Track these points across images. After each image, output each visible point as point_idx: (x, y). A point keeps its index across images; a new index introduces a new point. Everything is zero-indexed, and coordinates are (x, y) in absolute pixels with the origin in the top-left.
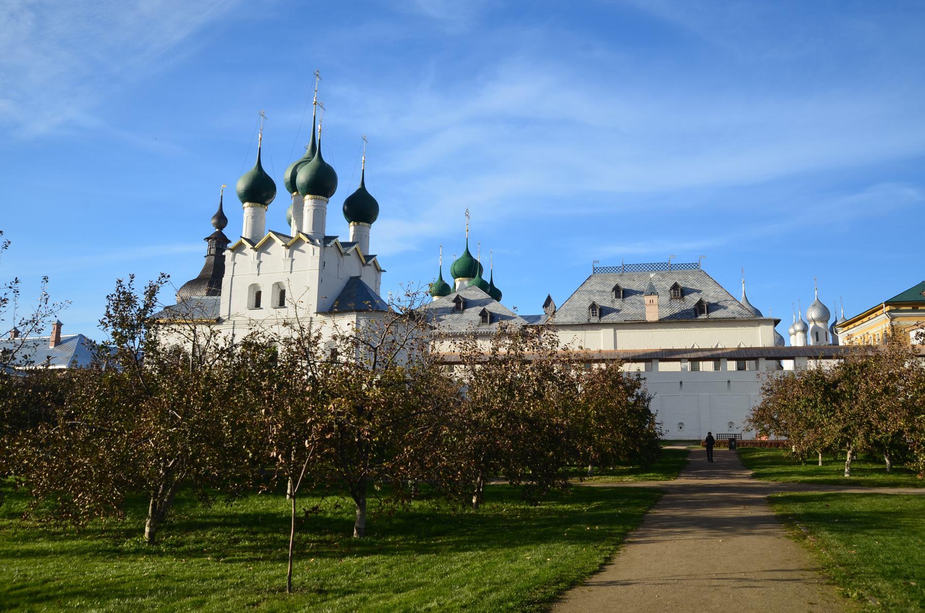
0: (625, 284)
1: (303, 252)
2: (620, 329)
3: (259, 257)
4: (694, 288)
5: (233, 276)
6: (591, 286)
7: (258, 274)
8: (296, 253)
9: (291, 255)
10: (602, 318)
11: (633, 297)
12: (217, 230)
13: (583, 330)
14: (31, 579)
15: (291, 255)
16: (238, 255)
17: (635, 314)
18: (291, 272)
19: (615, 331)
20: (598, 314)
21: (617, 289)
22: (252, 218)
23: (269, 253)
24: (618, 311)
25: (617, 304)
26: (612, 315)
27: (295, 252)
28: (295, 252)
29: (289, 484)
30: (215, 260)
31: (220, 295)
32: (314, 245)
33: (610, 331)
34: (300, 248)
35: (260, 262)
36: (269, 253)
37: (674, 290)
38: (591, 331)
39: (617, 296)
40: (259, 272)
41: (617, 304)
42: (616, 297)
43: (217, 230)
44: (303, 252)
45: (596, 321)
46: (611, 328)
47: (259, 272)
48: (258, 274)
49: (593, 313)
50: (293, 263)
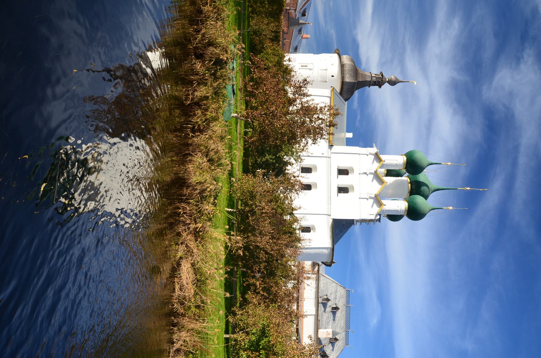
0: (339, 314)
1: (372, 206)
2: (315, 317)
3: (371, 173)
4: (335, 346)
5: (359, 154)
6: (340, 291)
7: (359, 174)
8: (372, 201)
9: (371, 198)
10: (321, 304)
11: (332, 316)
12: (387, 80)
13: (315, 297)
14: (149, 208)
15: (371, 198)
16: (373, 157)
17: (322, 321)
18: (360, 198)
19: (314, 315)
20: (324, 302)
21: (337, 308)
22: (396, 164)
23: (373, 181)
24: (325, 311)
25: (329, 309)
26: (323, 309)
27: (372, 200)
28: (372, 200)
29: (230, 210)
30: (368, 81)
31: (347, 145)
32: (376, 215)
33: (314, 312)
34: (374, 180)
35: (367, 175)
36: (373, 181)
37: (334, 339)
38: (314, 302)
39: (333, 308)
40: (361, 174)
41: (329, 309)
42: (332, 308)
43: (387, 80)
44: (372, 206)
45: (320, 301)
46: (316, 313)
47: (361, 174)
48: (360, 198)
49: (324, 299)
50: (366, 200)
